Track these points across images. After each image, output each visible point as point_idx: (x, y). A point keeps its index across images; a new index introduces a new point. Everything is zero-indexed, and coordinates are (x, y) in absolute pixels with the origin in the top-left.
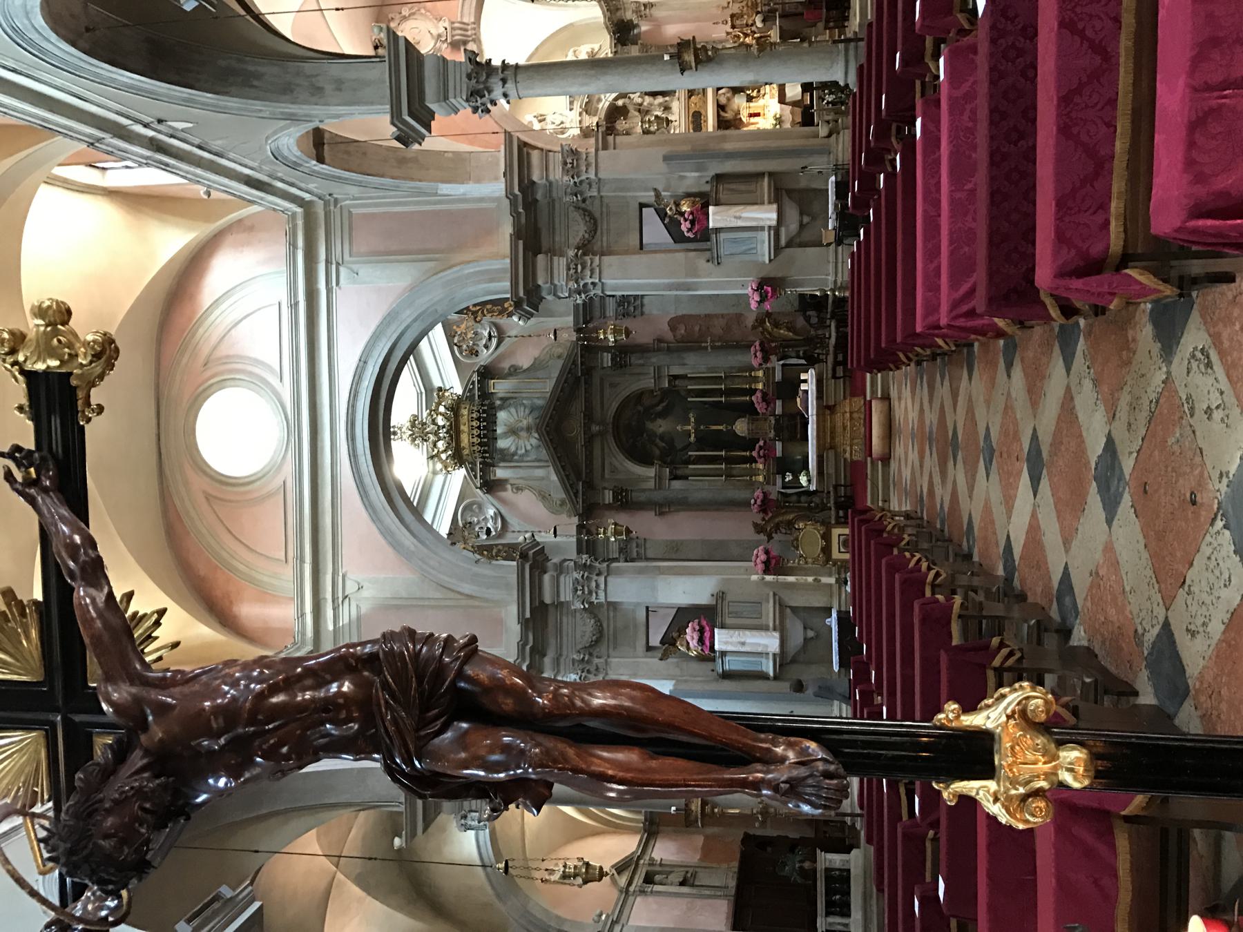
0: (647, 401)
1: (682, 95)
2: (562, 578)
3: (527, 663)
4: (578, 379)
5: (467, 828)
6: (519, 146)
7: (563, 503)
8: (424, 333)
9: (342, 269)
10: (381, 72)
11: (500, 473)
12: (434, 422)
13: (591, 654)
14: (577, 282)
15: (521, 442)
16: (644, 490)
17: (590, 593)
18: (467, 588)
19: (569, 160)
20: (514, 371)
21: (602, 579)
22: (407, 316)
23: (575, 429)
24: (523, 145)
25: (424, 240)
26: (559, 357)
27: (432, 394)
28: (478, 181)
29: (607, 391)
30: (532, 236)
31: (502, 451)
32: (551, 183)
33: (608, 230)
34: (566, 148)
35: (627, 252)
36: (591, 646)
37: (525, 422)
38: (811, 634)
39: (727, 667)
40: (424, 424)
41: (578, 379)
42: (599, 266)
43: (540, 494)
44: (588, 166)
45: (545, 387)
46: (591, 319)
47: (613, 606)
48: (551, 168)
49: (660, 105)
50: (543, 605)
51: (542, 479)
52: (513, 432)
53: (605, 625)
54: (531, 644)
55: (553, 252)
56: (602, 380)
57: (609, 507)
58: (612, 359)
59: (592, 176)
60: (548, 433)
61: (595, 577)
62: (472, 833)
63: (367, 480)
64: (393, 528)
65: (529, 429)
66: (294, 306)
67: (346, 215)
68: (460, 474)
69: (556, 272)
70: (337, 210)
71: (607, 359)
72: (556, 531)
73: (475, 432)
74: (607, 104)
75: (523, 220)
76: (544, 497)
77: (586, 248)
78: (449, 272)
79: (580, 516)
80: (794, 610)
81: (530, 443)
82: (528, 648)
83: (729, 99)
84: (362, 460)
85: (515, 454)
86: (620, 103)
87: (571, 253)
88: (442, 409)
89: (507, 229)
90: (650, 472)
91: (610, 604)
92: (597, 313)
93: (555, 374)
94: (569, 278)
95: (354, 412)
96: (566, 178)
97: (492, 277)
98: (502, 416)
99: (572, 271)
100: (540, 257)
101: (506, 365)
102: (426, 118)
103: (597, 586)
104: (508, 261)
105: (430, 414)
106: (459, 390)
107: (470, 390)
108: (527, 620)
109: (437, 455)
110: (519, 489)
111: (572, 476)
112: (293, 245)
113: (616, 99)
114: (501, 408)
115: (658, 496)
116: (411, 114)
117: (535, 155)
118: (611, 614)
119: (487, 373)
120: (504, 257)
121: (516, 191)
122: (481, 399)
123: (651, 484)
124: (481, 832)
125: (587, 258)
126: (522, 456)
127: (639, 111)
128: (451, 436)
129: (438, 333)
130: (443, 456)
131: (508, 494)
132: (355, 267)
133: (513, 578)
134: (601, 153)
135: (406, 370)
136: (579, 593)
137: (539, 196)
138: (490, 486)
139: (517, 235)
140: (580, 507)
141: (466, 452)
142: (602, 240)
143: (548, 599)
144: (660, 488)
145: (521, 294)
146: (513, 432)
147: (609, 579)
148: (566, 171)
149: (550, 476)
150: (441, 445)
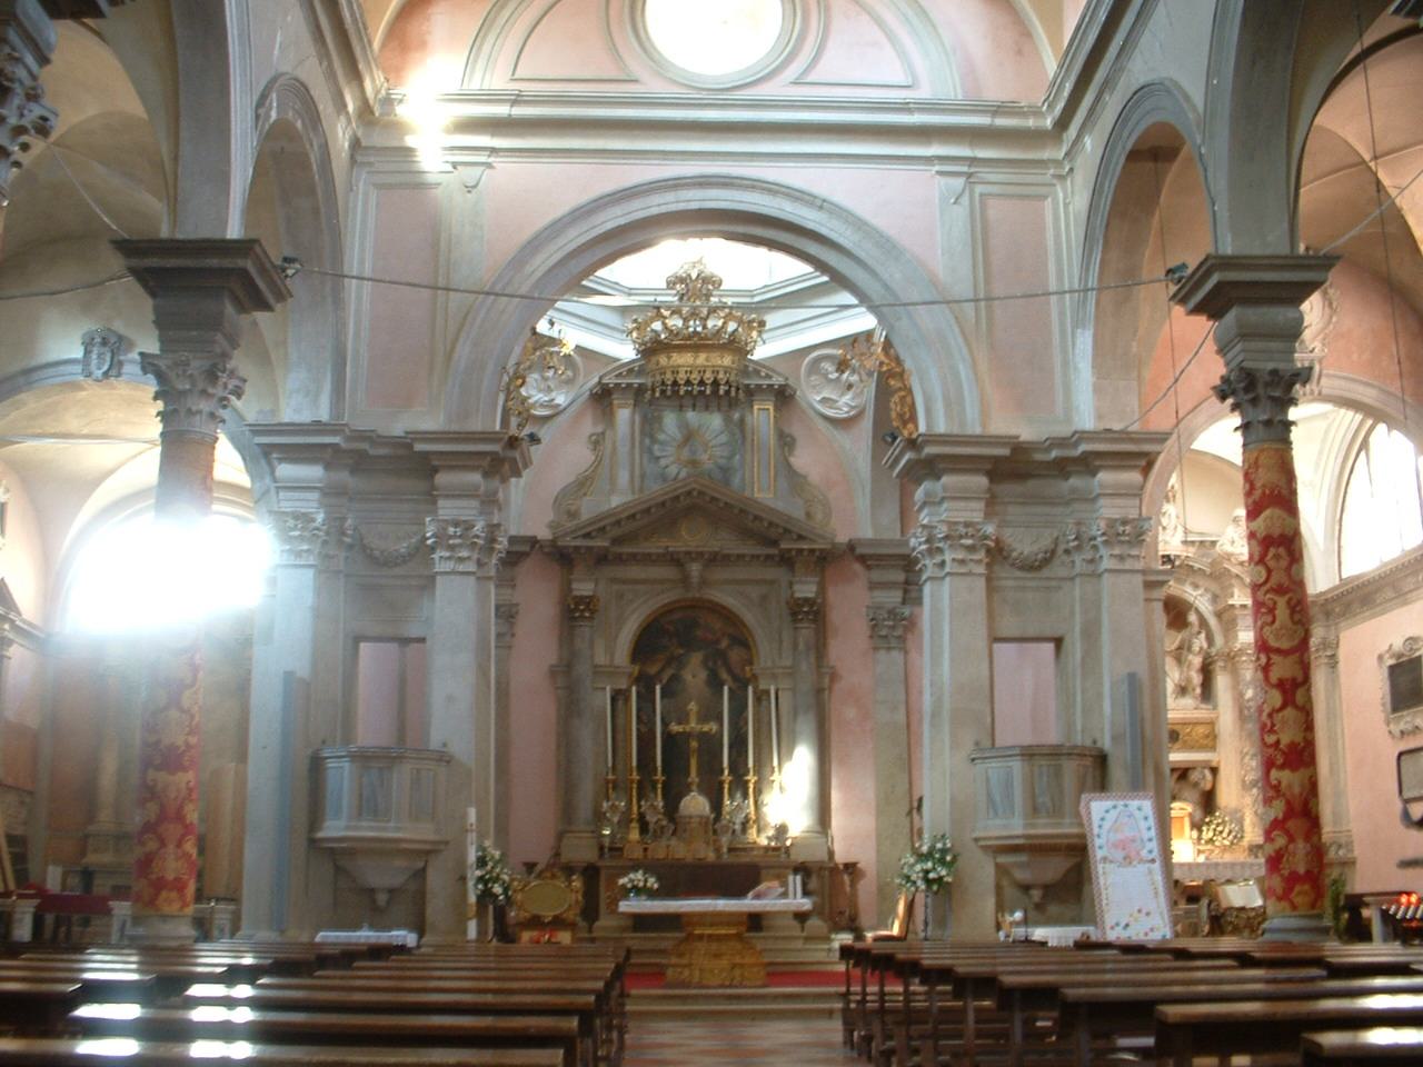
0: (735, 655)
1: (1203, 713)
2: (475, 503)
3: (343, 445)
4: (775, 543)
5: (88, 346)
6: (1146, 454)
7: (572, 515)
8: (864, 299)
9: (961, 181)
10: (1272, 242)
11: (624, 415)
12: (713, 310)
13: (351, 547)
14: (947, 538)
15: (671, 450)
16: (591, 646)
17: (452, 548)
18: (463, 351)
19: (1128, 528)
20: (786, 442)
21: (471, 567)
22: (893, 274)
23: (691, 538)
24: (1145, 462)
25: (998, 302)
26: (808, 515)
27: (754, 313)
28: (1097, 390)
29: (755, 592)
30: (1013, 469)
31: (659, 419)
32: (1094, 500)
33: (1024, 589)
34: (1146, 526)
35: (991, 616)
36: (364, 548)
37: (705, 457)
38: (382, 898)
39: (331, 764)
40: (708, 295)
41: (775, 543)
42: (969, 574)
43: (587, 478)
44: (1121, 558)
45: (762, 490)
46: (869, 568)
47: (429, 582)
48: (1118, 501)
49: (1189, 680)
50: (435, 470)
51: (612, 480)
52: (689, 436)
53: (398, 571)
54: (372, 452)
55: (992, 503)
56: (772, 582)
57: (566, 589)
58: (806, 600)
59: (1107, 564)
60: (689, 493)
61: (475, 556)
62: (78, 353)
63: (636, 204)
64: (561, 241)
65: (694, 463)
66: (905, 107)
67: (1042, 190)
68: (626, 352)
69: (951, 506)
70: (1048, 178)
71: (806, 589)
72: (528, 507)
73: (695, 377)
74: (1191, 599)
75: (1039, 457)
76: (583, 484)
77: (997, 553)
78: (960, 340)
79: (553, 542)
80: (420, 874)
81: (672, 465)
82: (365, 446)
83: (1196, 785)
84: (670, 197)
85: (654, 440)
86: (1192, 618)
87: (990, 529)
88: (732, 326)
89: (1026, 433)
90: (622, 654)
91: (432, 579)
92: (876, 575)
93: (780, 506)
94: (951, 524)
95: (746, 188)
96: (1102, 524)
97: (954, 403)
98: (715, 421)
99: (963, 530)
100: (983, 481)
101: (796, 429)
102: (1212, 307)
103: (461, 560)
104: (978, 431)
105: (724, 306)
106: (761, 352)
107: (757, 372)
108: (409, 446)
109: (659, 316)
110: (596, 442)
111: (616, 532)
112: (998, 109)
113: (1198, 612)
114: (728, 420)
115: (583, 669)
116: (1219, 286)
117: (1134, 477)
118: (414, 583)
119: (783, 397)
120: (984, 425)
121: (1083, 447)
122: (738, 390)
123: (601, 658)
124: (78, 368)
125: (981, 555)
126: (650, 451)
127: (1180, 648)
128: (690, 337)
129: (863, 321)
130: (657, 326)
131: (589, 426)
132: (965, 200)
133: (476, 425)
134: (1139, 579)
135: (806, 268)
136: (451, 530)
137: (1074, 481)
138: (603, 397)
139: (1019, 449)
140: (569, 542)
141: (663, 360)
142: (1008, 578)
143: (442, 479)
144: (595, 673)
145: (929, 450)
146: (689, 436)
147: (472, 579)
148: (1111, 523)
149: (618, 496)
150: (676, 322)
